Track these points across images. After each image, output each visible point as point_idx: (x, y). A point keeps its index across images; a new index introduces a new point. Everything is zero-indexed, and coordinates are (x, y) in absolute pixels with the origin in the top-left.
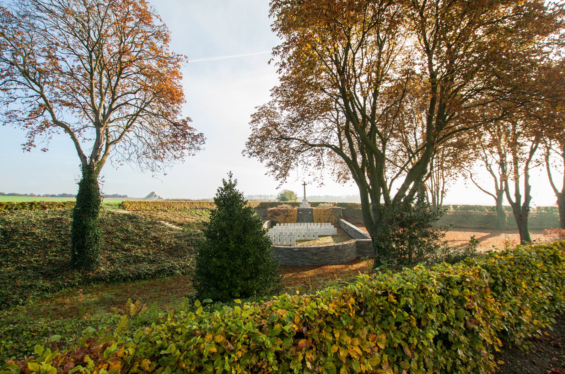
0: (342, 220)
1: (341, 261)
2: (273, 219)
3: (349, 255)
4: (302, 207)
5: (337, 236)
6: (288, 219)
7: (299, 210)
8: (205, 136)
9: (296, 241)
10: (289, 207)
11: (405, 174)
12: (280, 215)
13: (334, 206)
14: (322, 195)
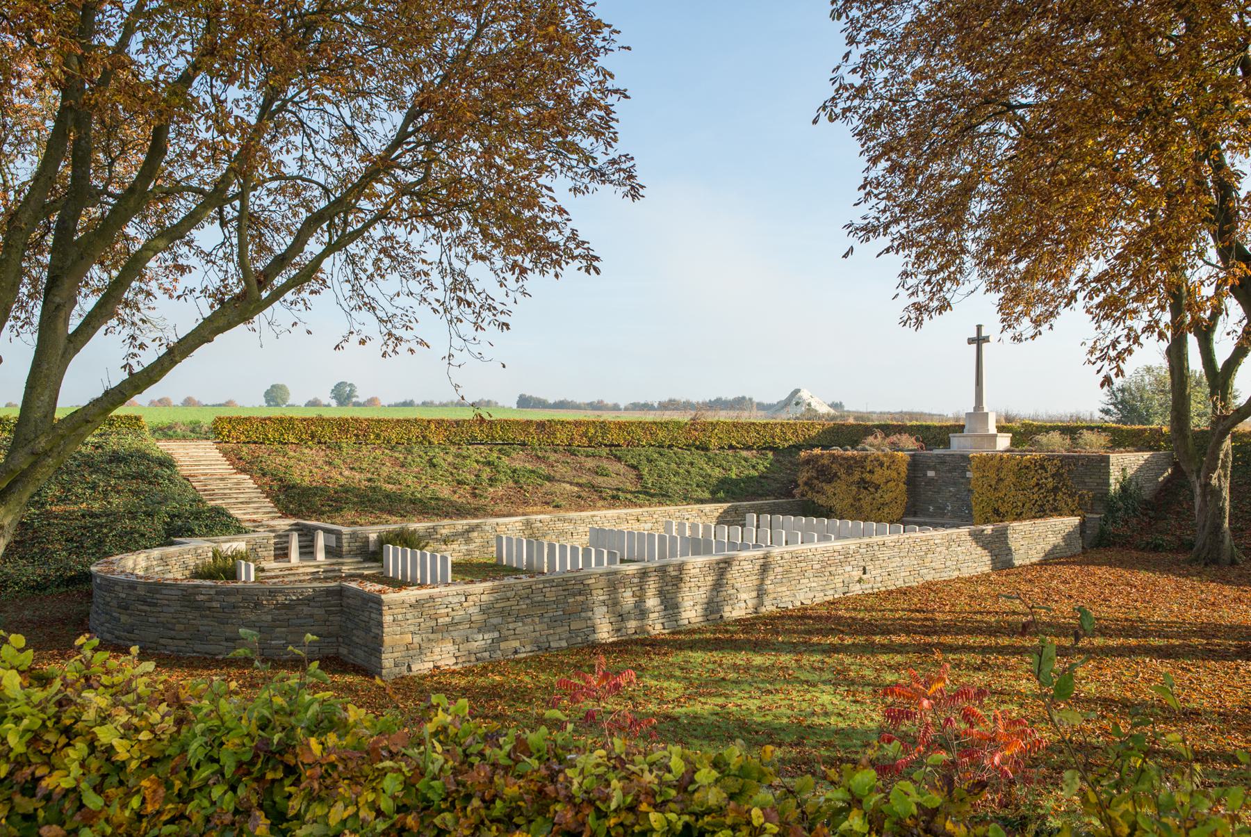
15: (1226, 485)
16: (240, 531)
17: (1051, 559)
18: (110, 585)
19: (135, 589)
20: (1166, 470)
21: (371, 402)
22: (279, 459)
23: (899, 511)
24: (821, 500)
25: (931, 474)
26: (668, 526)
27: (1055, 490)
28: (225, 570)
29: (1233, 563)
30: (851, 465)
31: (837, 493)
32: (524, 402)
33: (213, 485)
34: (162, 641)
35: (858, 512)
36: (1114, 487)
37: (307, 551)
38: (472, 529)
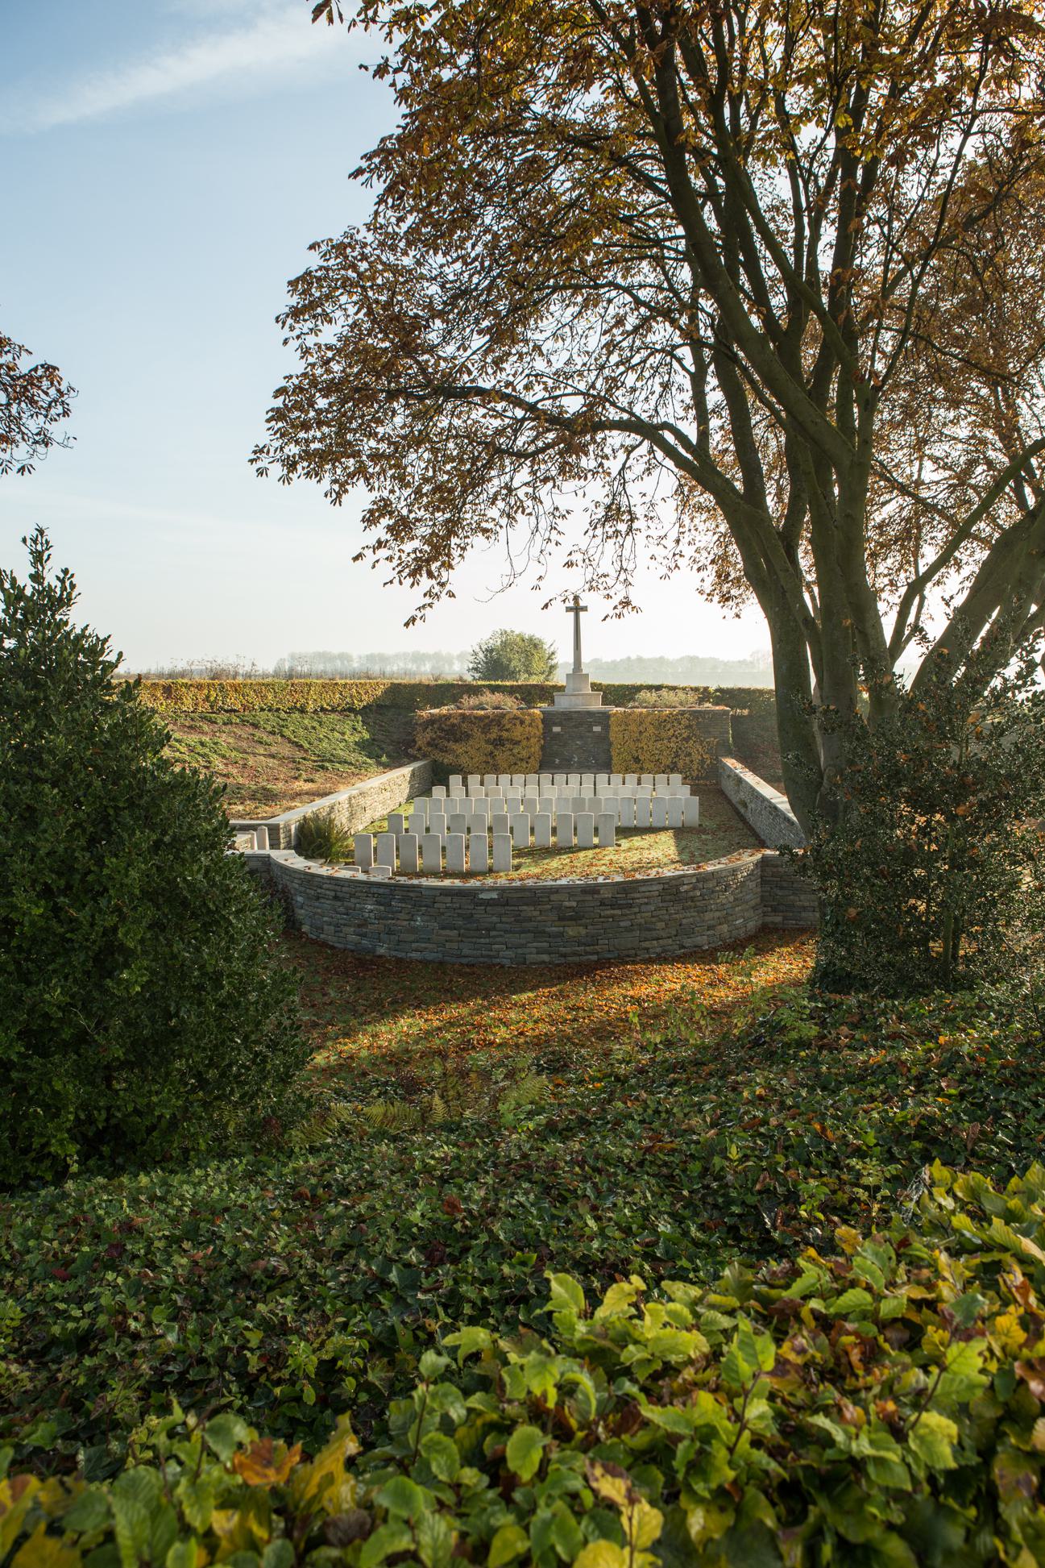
0: (731, 762)
1: (688, 942)
2: (438, 756)
3: (725, 919)
4: (562, 703)
5: (700, 830)
6: (501, 757)
7: (548, 720)
8: (67, 376)
9: (519, 853)
10: (510, 704)
11: (973, 557)
12: (468, 737)
13: (701, 701)
14: (672, 655)
19: (598, 892)
34: (646, 944)
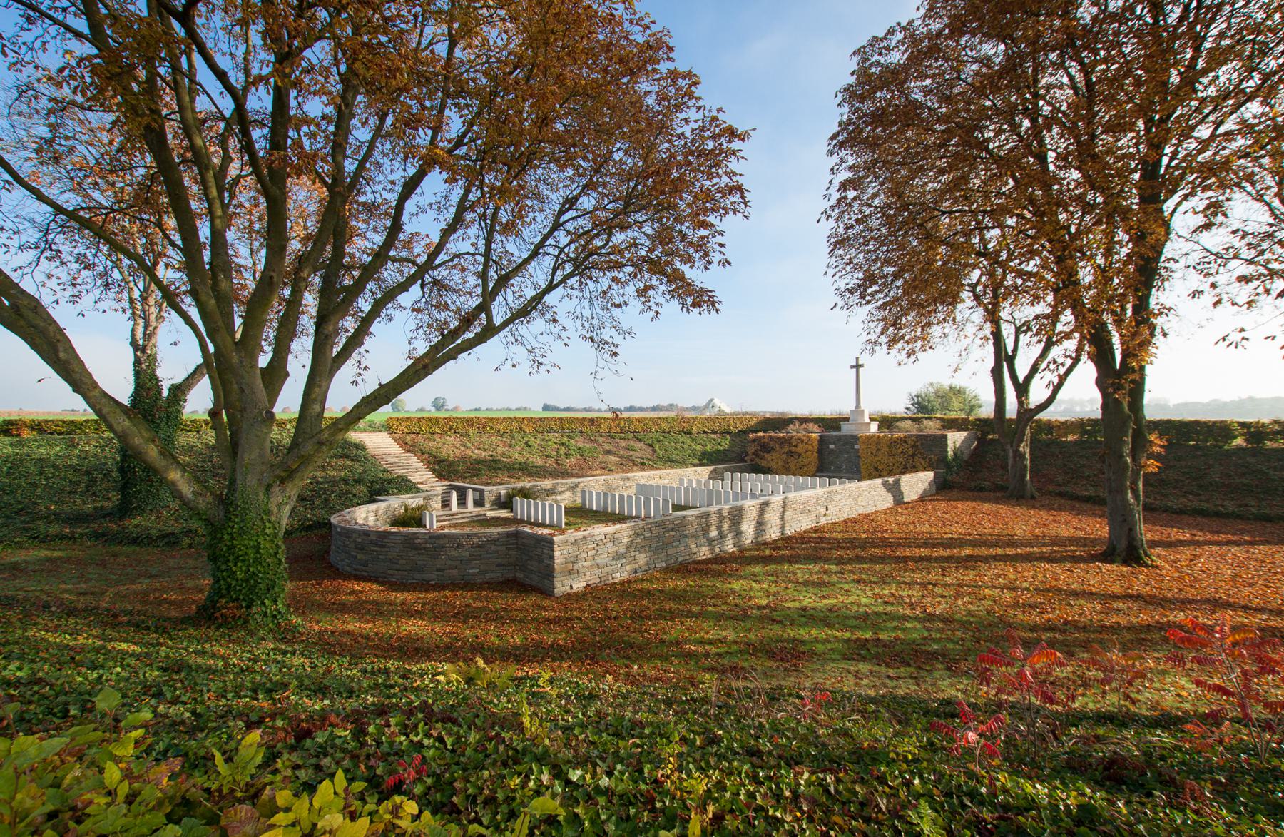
15: (1028, 450)
16: (418, 490)
17: (923, 498)
18: (348, 533)
20: (992, 440)
21: (455, 409)
22: (431, 444)
23: (814, 469)
24: (763, 463)
25: (832, 446)
26: (681, 481)
27: (913, 455)
28: (414, 518)
29: (1033, 498)
30: (782, 442)
31: (773, 459)
32: (546, 408)
33: (391, 460)
35: (787, 471)
36: (950, 453)
37: (462, 502)
38: (577, 485)
